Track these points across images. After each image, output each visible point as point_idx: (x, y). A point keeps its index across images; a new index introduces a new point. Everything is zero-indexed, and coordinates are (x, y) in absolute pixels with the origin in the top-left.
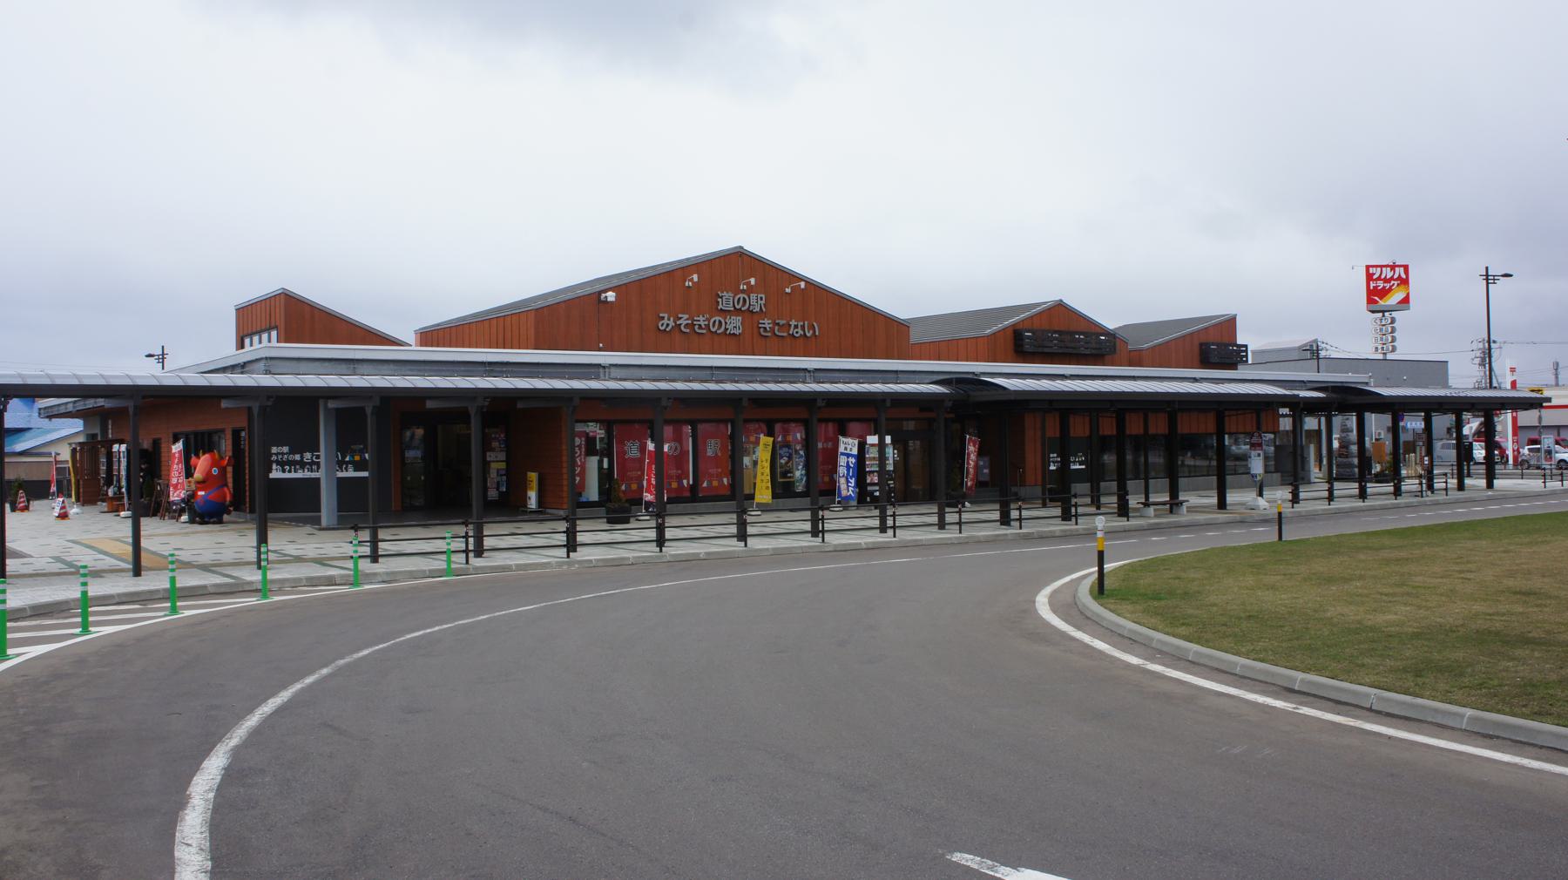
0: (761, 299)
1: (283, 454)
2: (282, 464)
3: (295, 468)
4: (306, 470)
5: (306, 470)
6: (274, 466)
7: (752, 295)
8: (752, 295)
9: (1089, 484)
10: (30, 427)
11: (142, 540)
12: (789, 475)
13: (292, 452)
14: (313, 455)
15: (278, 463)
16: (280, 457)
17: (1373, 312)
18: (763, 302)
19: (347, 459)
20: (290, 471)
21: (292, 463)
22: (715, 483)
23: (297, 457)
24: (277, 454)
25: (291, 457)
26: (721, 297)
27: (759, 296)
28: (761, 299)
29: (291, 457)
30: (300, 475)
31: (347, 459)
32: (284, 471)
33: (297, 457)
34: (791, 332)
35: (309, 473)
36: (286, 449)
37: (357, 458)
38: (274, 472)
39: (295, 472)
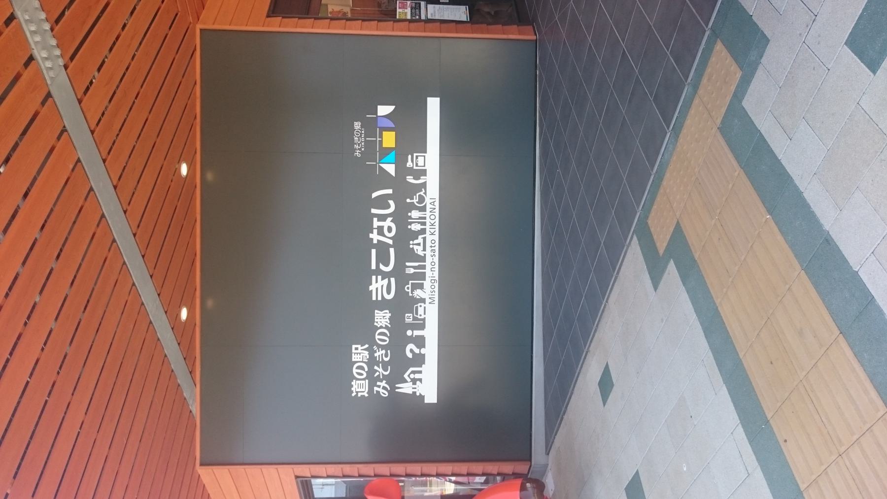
0: (357, 349)
1: (372, 361)
3: (413, 327)
4: (418, 293)
5: (418, 293)
6: (406, 388)
7: (353, 360)
8: (353, 360)
13: (367, 335)
14: (378, 272)
15: (396, 378)
16: (380, 370)
18: (359, 346)
19: (391, 169)
20: (420, 342)
21: (398, 329)
23: (382, 318)
24: (373, 380)
25: (382, 338)
26: (357, 392)
27: (354, 351)
28: (357, 349)
29: (382, 338)
30: (430, 313)
31: (391, 169)
32: (419, 360)
33: (382, 318)
34: (390, 242)
35: (427, 284)
36: (359, 354)
37: (389, 139)
38: (420, 389)
39: (422, 326)
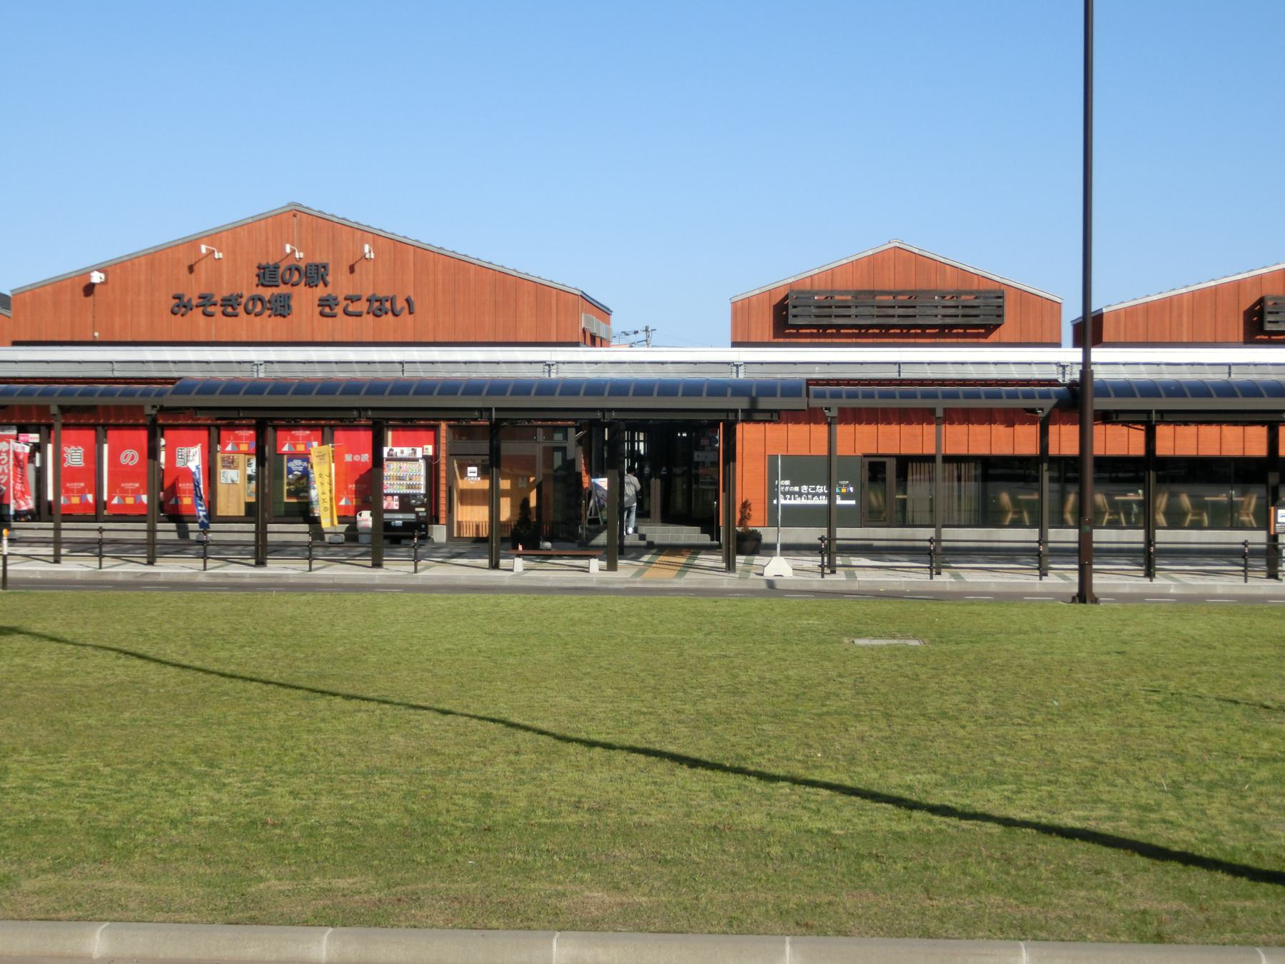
1: (785, 486)
2: (784, 494)
9: (1077, 530)
10: (175, 478)
11: (1077, 581)
12: (302, 494)
13: (793, 485)
17: (306, 267)
20: (790, 499)
21: (793, 493)
22: (130, 501)
25: (792, 489)
29: (792, 489)
33: (796, 489)
